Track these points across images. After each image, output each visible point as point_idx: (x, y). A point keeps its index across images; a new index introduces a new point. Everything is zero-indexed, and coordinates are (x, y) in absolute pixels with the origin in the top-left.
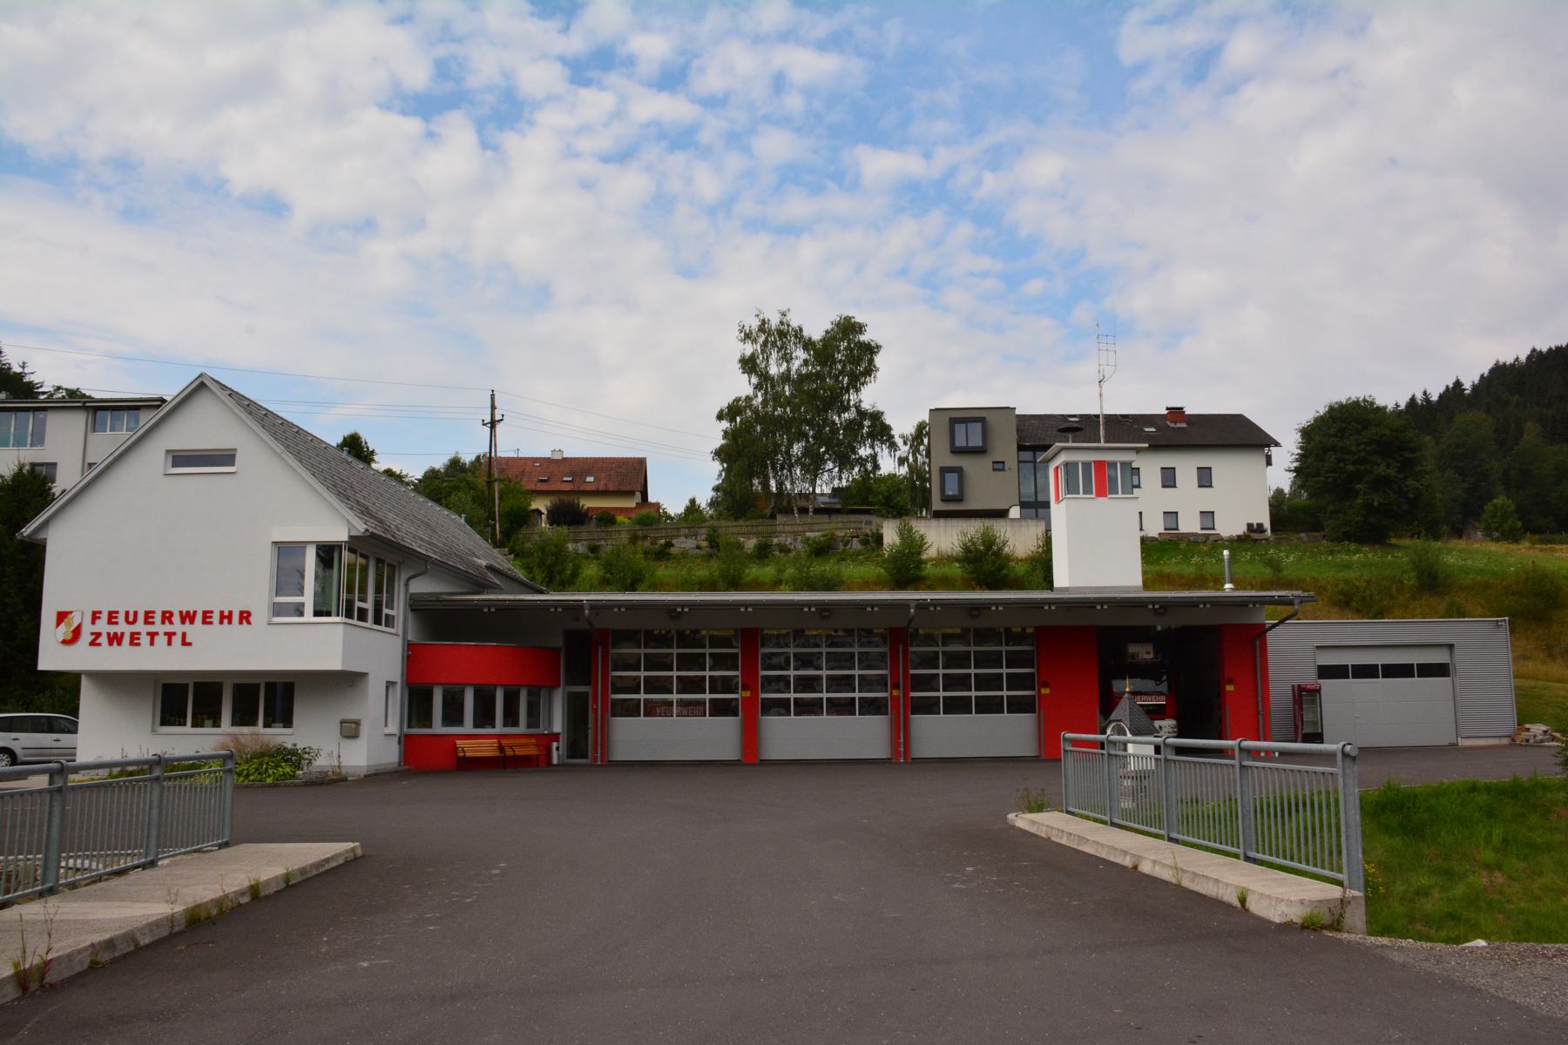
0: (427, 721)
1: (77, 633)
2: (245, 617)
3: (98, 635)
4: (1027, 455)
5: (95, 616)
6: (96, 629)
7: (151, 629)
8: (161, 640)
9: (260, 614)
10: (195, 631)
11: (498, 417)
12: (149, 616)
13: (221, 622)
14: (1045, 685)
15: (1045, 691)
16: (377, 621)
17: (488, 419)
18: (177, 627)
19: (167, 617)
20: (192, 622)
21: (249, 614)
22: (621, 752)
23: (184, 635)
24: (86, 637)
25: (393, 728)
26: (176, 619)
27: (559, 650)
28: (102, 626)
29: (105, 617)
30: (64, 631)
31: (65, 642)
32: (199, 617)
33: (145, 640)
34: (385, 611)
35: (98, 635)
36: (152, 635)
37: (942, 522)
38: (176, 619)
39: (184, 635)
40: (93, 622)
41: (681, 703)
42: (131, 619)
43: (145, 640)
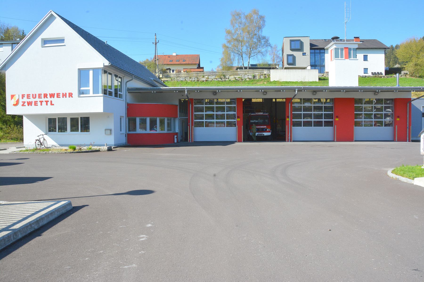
0: (135, 129)
1: (18, 102)
2: (71, 95)
3: (24, 102)
4: (313, 51)
5: (23, 96)
6: (23, 100)
7: (41, 100)
8: (44, 103)
9: (75, 93)
10: (55, 100)
11: (157, 41)
12: (40, 95)
13: (63, 97)
14: (337, 117)
15: (337, 119)
16: (116, 95)
17: (154, 42)
18: (49, 99)
19: (45, 96)
20: (54, 97)
21: (72, 94)
22: (198, 139)
23: (51, 101)
24: (21, 103)
25: (123, 131)
26: (48, 96)
27: (177, 105)
28: (25, 99)
29: (26, 96)
30: (14, 101)
31: (14, 105)
32: (56, 96)
33: (39, 103)
34: (119, 93)
35: (24, 102)
36: (41, 102)
37: (288, 70)
38: (48, 96)
39: (51, 101)
40: (23, 98)
41: (217, 123)
42: (34, 96)
43: (39, 103)
